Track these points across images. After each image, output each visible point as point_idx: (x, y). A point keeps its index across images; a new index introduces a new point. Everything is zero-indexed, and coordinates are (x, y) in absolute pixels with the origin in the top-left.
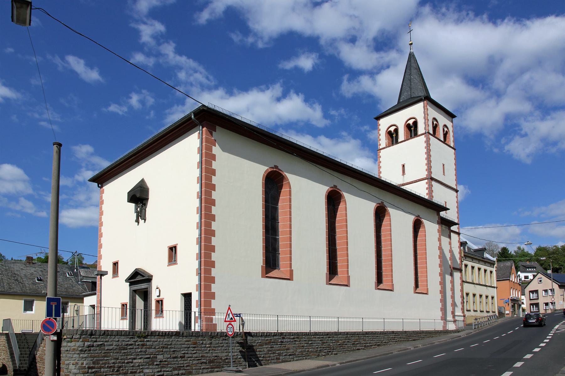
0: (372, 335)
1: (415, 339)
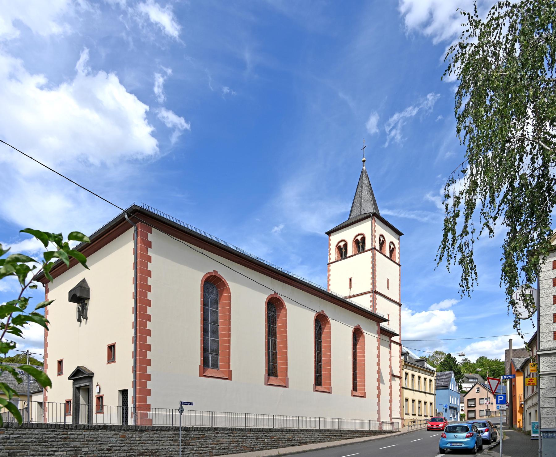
0: (307, 433)
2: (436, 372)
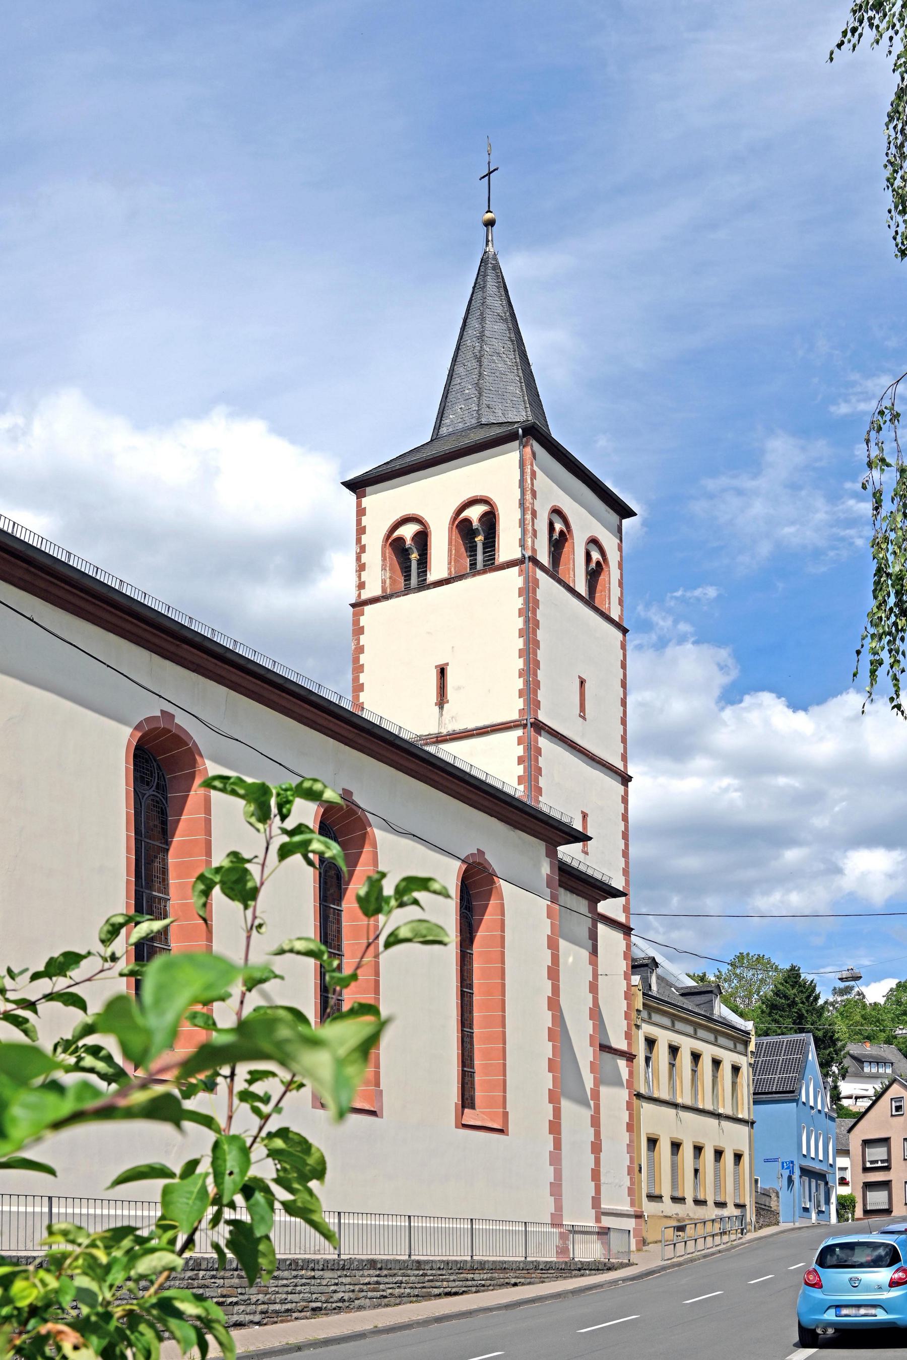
0: (294, 1273)
1: (454, 1290)
2: (753, 1038)
